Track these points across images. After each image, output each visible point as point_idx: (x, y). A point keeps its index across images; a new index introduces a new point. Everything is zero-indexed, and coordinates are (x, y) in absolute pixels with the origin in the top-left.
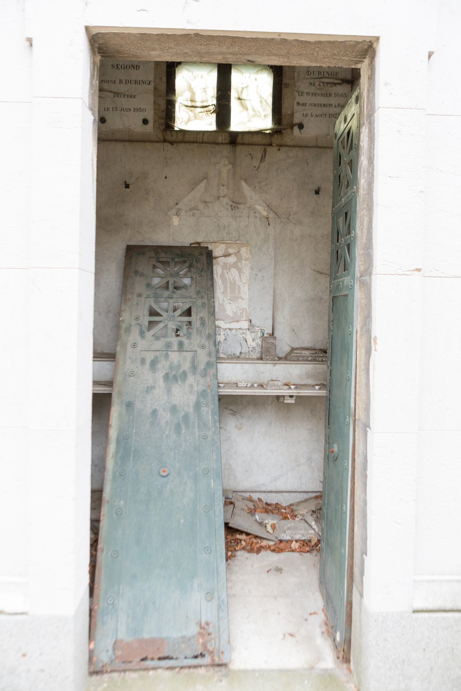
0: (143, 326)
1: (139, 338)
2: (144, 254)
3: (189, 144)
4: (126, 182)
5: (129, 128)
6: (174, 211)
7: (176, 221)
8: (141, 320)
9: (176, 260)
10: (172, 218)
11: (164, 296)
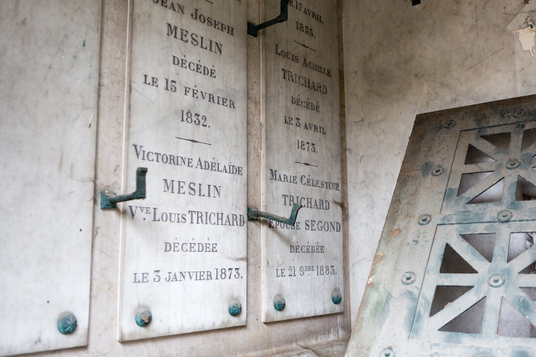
0: (421, 300)
1: (404, 333)
2: (450, 125)
8: (418, 283)
9: (528, 127)
10: (517, 35)
11: (487, 218)
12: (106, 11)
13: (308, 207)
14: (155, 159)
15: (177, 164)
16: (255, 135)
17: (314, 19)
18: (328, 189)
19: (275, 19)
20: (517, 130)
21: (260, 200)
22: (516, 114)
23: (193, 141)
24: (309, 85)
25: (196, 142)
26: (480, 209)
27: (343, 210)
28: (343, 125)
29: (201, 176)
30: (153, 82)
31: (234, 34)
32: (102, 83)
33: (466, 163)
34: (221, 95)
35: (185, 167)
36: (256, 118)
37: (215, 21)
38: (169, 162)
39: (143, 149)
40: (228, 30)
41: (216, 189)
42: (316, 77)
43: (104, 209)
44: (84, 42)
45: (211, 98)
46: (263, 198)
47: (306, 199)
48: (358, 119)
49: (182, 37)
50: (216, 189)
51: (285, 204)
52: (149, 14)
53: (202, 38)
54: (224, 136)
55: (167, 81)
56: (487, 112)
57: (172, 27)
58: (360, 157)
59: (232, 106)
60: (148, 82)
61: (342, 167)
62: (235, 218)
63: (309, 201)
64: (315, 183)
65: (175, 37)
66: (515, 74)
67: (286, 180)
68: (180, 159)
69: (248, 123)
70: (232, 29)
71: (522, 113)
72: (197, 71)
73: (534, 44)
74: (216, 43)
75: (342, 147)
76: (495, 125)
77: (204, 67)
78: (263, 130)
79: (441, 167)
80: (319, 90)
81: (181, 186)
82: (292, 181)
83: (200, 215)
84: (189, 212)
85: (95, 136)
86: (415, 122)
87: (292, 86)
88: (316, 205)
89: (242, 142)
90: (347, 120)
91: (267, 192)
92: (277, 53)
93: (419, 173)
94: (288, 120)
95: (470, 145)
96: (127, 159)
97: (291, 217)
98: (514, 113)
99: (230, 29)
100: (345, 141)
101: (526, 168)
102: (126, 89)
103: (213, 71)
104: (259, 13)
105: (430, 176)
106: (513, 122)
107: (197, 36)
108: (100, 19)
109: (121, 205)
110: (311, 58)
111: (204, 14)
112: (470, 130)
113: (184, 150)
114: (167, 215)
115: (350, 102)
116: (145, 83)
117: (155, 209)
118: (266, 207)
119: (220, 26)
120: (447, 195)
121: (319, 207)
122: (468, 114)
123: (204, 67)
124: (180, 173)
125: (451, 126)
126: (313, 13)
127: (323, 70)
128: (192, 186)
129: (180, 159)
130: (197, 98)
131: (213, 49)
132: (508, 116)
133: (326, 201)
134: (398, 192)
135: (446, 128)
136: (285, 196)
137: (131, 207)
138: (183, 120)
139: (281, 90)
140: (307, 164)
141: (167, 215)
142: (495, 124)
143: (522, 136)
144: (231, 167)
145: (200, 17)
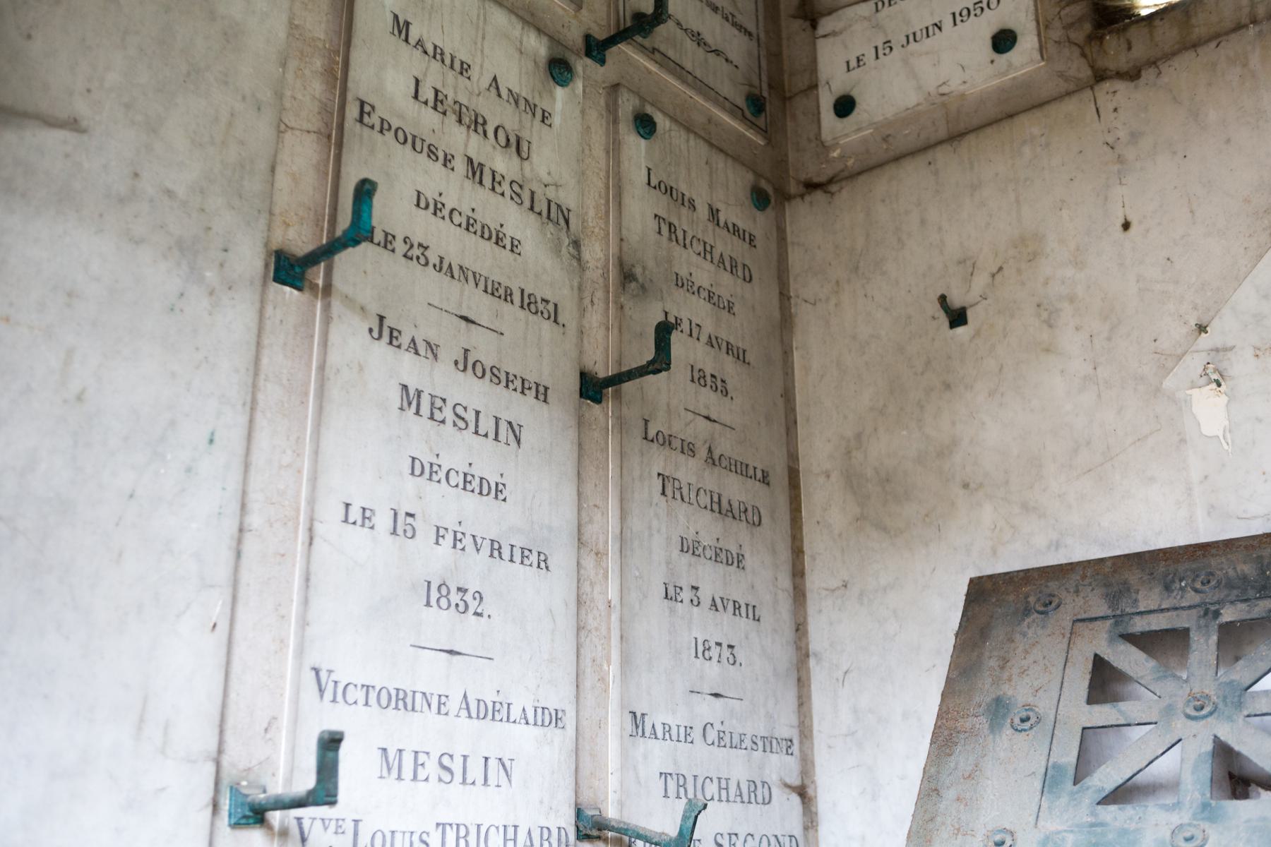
2: (1049, 605)
3: (1213, 45)
4: (943, 299)
5: (944, 89)
6: (1194, 363)
7: (1209, 411)
9: (1228, 615)
10: (1188, 402)
12: (265, 361)
13: (720, 800)
14: (362, 701)
15: (413, 709)
16: (597, 629)
17: (731, 357)
18: (768, 753)
19: (643, 367)
20: (1202, 622)
21: (606, 787)
22: (1198, 585)
23: (451, 652)
24: (721, 508)
25: (459, 653)
26: (1131, 819)
27: (803, 803)
28: (799, 595)
29: (467, 737)
30: (364, 518)
31: (549, 399)
32: (246, 525)
33: (1091, 700)
34: (519, 542)
35: (431, 716)
36: (597, 589)
37: (507, 373)
38: (393, 704)
39: (334, 677)
40: (537, 391)
41: (504, 765)
42: (736, 489)
43: (235, 826)
44: (212, 434)
45: (496, 549)
46: (613, 782)
47: (716, 781)
48: (835, 583)
49: (432, 414)
50: (504, 765)
51: (666, 796)
52: (360, 365)
53: (478, 413)
54: (524, 637)
55: (396, 514)
56: (1133, 577)
57: (412, 392)
58: (840, 674)
59: (543, 565)
60: (351, 520)
61: (800, 697)
62: (545, 836)
63: (724, 786)
64: (736, 740)
65: (417, 413)
66: (1189, 490)
67: (667, 736)
68: (419, 696)
69: (579, 602)
70: (546, 389)
71: (1213, 583)
72: (465, 489)
73: (1227, 423)
74: (510, 423)
75: (798, 648)
76: (1153, 609)
77: (481, 479)
78: (615, 617)
79: (1031, 710)
80: (743, 518)
81: (420, 762)
82: (682, 738)
83: (462, 833)
84: (438, 825)
85: (224, 650)
86: (968, 595)
87: (682, 510)
88: (741, 795)
89: (565, 649)
90: (808, 585)
91: (623, 768)
92: (646, 438)
93: (982, 723)
94: (671, 592)
95: (1096, 655)
96: (296, 701)
97: (681, 833)
98: (1194, 580)
99: (541, 389)
100: (805, 633)
101: (1230, 719)
102: (302, 535)
103: (501, 487)
104: (607, 350)
105: (1008, 731)
106: (1192, 603)
107: (465, 409)
108: (250, 381)
109: (275, 817)
110: (725, 446)
111: (482, 359)
112: (1096, 619)
113: (429, 674)
114: (384, 836)
115: (814, 541)
116: (346, 521)
117: (356, 821)
118: (621, 804)
119: (518, 383)
120: (1050, 780)
121: (746, 799)
122: (1087, 581)
123: (481, 479)
124: (418, 732)
125: (1051, 607)
126: (728, 343)
127: (751, 472)
128: (446, 761)
129: (418, 696)
130: (463, 549)
131: (502, 437)
132: (1182, 589)
133: (764, 783)
134: (933, 770)
135: (1039, 612)
136: (665, 775)
137: (299, 819)
138: (428, 604)
139: (655, 523)
140: (716, 695)
141: (384, 836)
142: (1152, 608)
143: (1215, 638)
144: (539, 711)
145: (474, 365)
